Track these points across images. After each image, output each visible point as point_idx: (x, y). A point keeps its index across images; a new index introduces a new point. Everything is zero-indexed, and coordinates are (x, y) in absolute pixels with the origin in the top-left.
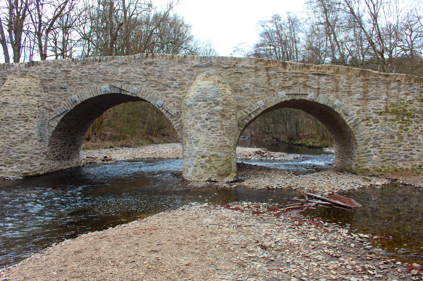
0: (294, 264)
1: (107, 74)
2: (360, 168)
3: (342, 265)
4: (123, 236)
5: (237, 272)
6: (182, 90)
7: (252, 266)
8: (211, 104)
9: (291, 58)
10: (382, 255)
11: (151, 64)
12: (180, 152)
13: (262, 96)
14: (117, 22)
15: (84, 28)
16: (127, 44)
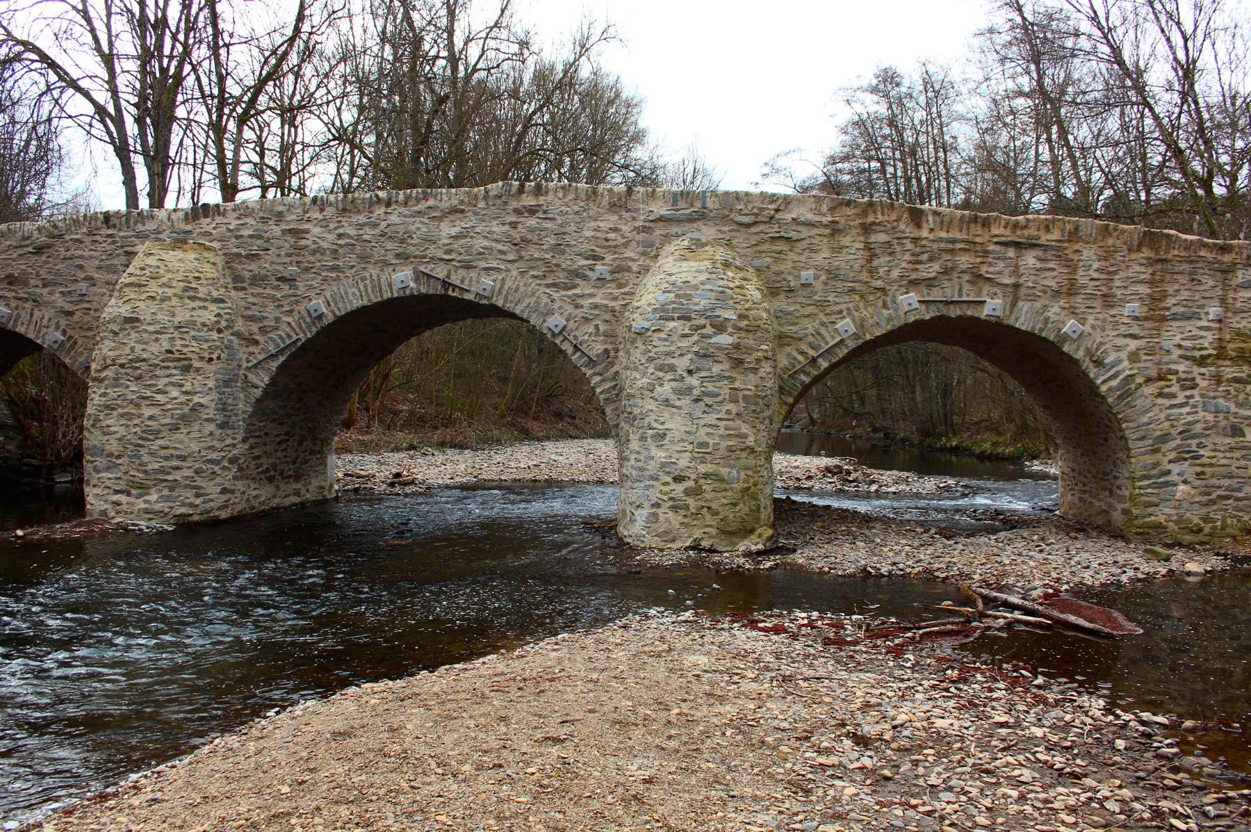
0: (950, 789)
1: (409, 241)
2: (1136, 522)
3: (1090, 799)
4: (464, 695)
5: (787, 805)
6: (620, 286)
7: (831, 792)
8: (704, 327)
9: (930, 195)
10: (1211, 776)
11: (532, 211)
12: (608, 465)
13: (851, 305)
14: (433, 91)
15: (339, 109)
16: (458, 155)
